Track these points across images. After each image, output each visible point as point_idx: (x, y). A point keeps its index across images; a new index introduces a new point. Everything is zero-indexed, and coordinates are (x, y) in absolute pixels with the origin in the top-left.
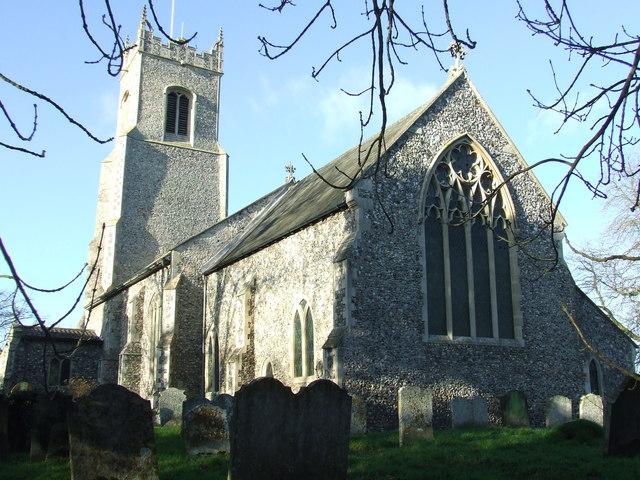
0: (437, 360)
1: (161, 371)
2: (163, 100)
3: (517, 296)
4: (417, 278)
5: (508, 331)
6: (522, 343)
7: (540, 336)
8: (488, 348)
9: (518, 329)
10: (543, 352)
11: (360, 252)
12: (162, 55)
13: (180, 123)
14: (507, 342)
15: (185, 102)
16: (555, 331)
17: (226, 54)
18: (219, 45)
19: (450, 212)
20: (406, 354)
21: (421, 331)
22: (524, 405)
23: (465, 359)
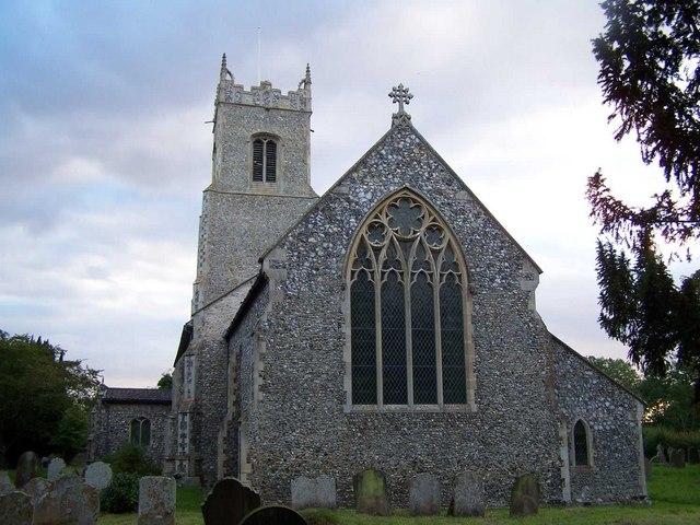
0: (361, 431)
1: (237, 403)
2: (250, 148)
3: (471, 357)
4: (338, 347)
5: (457, 393)
6: (474, 408)
7: (500, 398)
8: (428, 416)
9: (471, 393)
10: (502, 416)
11: (270, 325)
12: (244, 101)
13: (261, 173)
14: (453, 408)
15: (272, 146)
16: (520, 393)
17: (315, 90)
18: (307, 82)
19: (413, 274)
20: (323, 427)
21: (343, 402)
22: (382, 484)
23: (397, 428)
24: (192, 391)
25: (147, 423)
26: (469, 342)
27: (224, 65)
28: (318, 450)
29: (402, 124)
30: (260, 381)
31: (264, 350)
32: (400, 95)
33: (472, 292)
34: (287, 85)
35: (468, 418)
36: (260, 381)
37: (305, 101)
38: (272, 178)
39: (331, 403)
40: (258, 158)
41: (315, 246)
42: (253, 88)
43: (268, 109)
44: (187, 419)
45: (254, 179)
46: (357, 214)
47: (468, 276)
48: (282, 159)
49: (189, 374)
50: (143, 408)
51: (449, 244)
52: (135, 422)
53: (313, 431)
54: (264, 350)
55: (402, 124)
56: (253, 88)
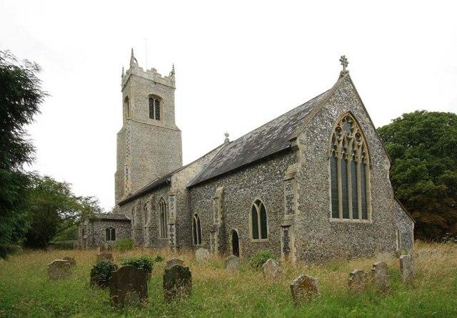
15: (158, 103)
18: (173, 73)
24: (175, 213)
25: (114, 230)
26: (331, 198)
27: (132, 54)
28: (321, 240)
29: (345, 77)
30: (298, 205)
31: (299, 188)
32: (344, 61)
33: (371, 167)
34: (164, 72)
35: (368, 226)
36: (298, 205)
37: (173, 82)
38: (158, 118)
39: (325, 218)
40: (151, 108)
41: (317, 135)
42: (147, 70)
43: (155, 83)
44: (174, 227)
45: (150, 118)
46: (332, 121)
47: (370, 160)
48: (163, 110)
49: (172, 205)
50: (111, 223)
51: (363, 143)
52: (107, 230)
53: (318, 231)
54: (299, 188)
55: (345, 77)
56: (147, 70)
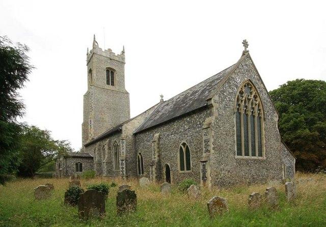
15: (112, 73)
18: (123, 52)
24: (125, 152)
25: (81, 164)
27: (94, 39)
28: (229, 172)
29: (246, 55)
30: (213, 146)
31: (213, 134)
32: (245, 44)
33: (264, 119)
34: (117, 51)
35: (263, 161)
36: (213, 146)
37: (123, 59)
38: (113, 84)
39: (232, 155)
40: (108, 77)
41: (226, 96)
42: (105, 50)
43: (111, 59)
44: (124, 162)
45: (107, 84)
46: (237, 87)
47: (264, 114)
48: (117, 78)
49: (123, 146)
50: (80, 159)
51: (259, 102)
52: (77, 164)
53: (227, 165)
54: (213, 134)
55: (246, 55)
56: (105, 50)
